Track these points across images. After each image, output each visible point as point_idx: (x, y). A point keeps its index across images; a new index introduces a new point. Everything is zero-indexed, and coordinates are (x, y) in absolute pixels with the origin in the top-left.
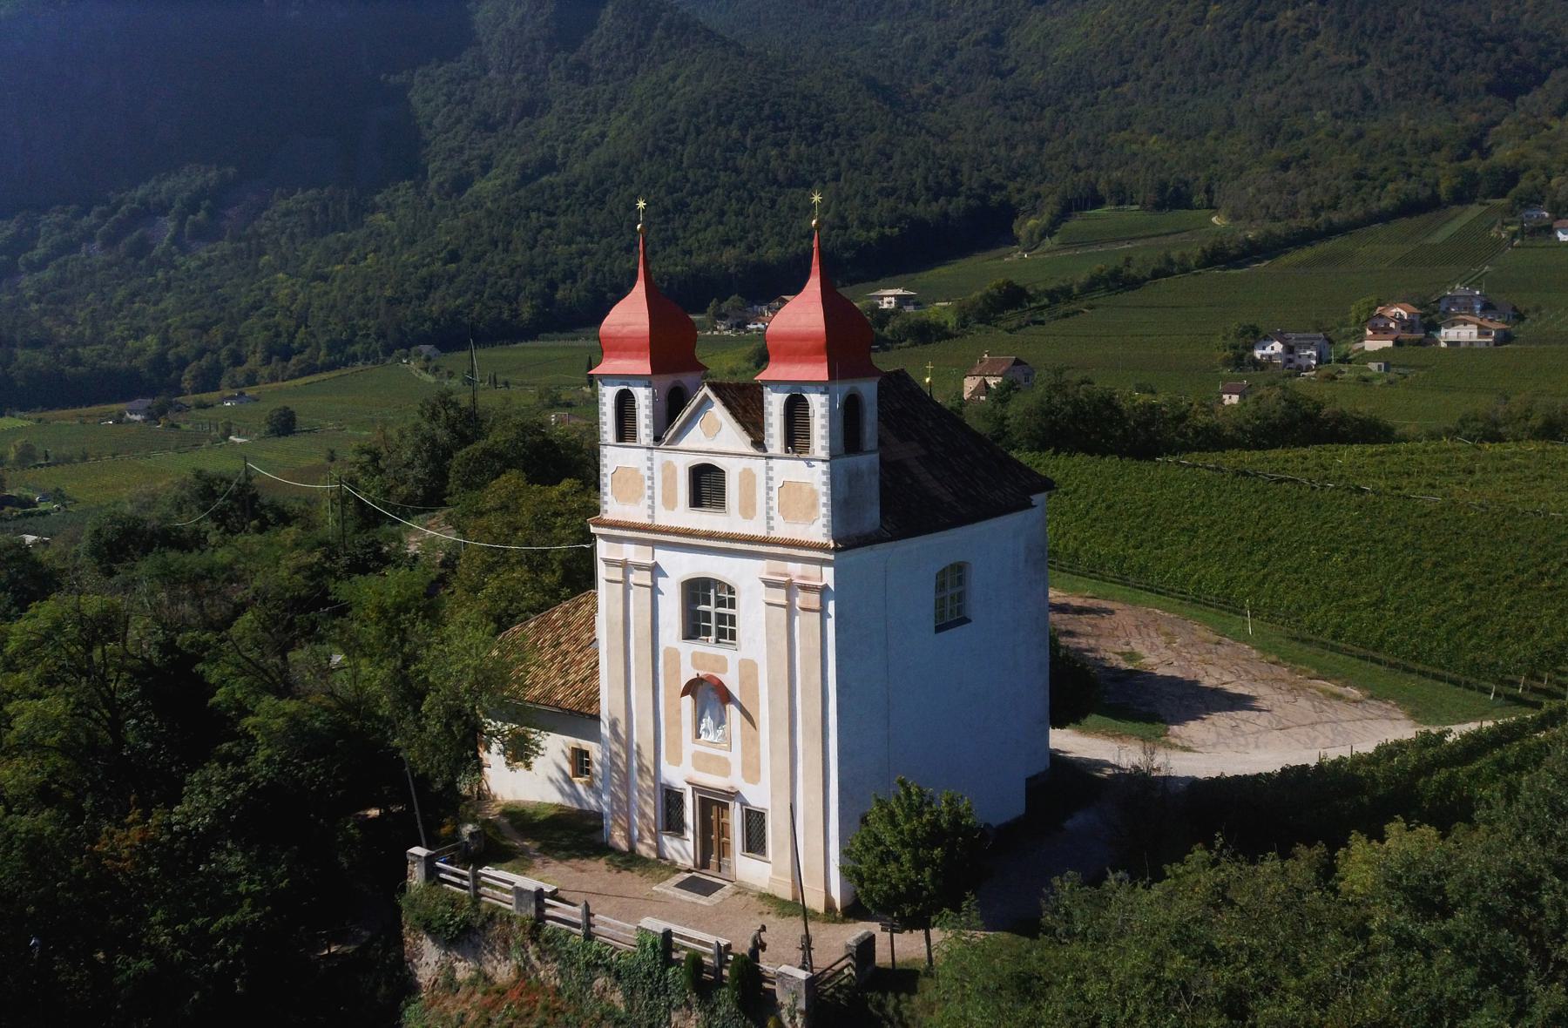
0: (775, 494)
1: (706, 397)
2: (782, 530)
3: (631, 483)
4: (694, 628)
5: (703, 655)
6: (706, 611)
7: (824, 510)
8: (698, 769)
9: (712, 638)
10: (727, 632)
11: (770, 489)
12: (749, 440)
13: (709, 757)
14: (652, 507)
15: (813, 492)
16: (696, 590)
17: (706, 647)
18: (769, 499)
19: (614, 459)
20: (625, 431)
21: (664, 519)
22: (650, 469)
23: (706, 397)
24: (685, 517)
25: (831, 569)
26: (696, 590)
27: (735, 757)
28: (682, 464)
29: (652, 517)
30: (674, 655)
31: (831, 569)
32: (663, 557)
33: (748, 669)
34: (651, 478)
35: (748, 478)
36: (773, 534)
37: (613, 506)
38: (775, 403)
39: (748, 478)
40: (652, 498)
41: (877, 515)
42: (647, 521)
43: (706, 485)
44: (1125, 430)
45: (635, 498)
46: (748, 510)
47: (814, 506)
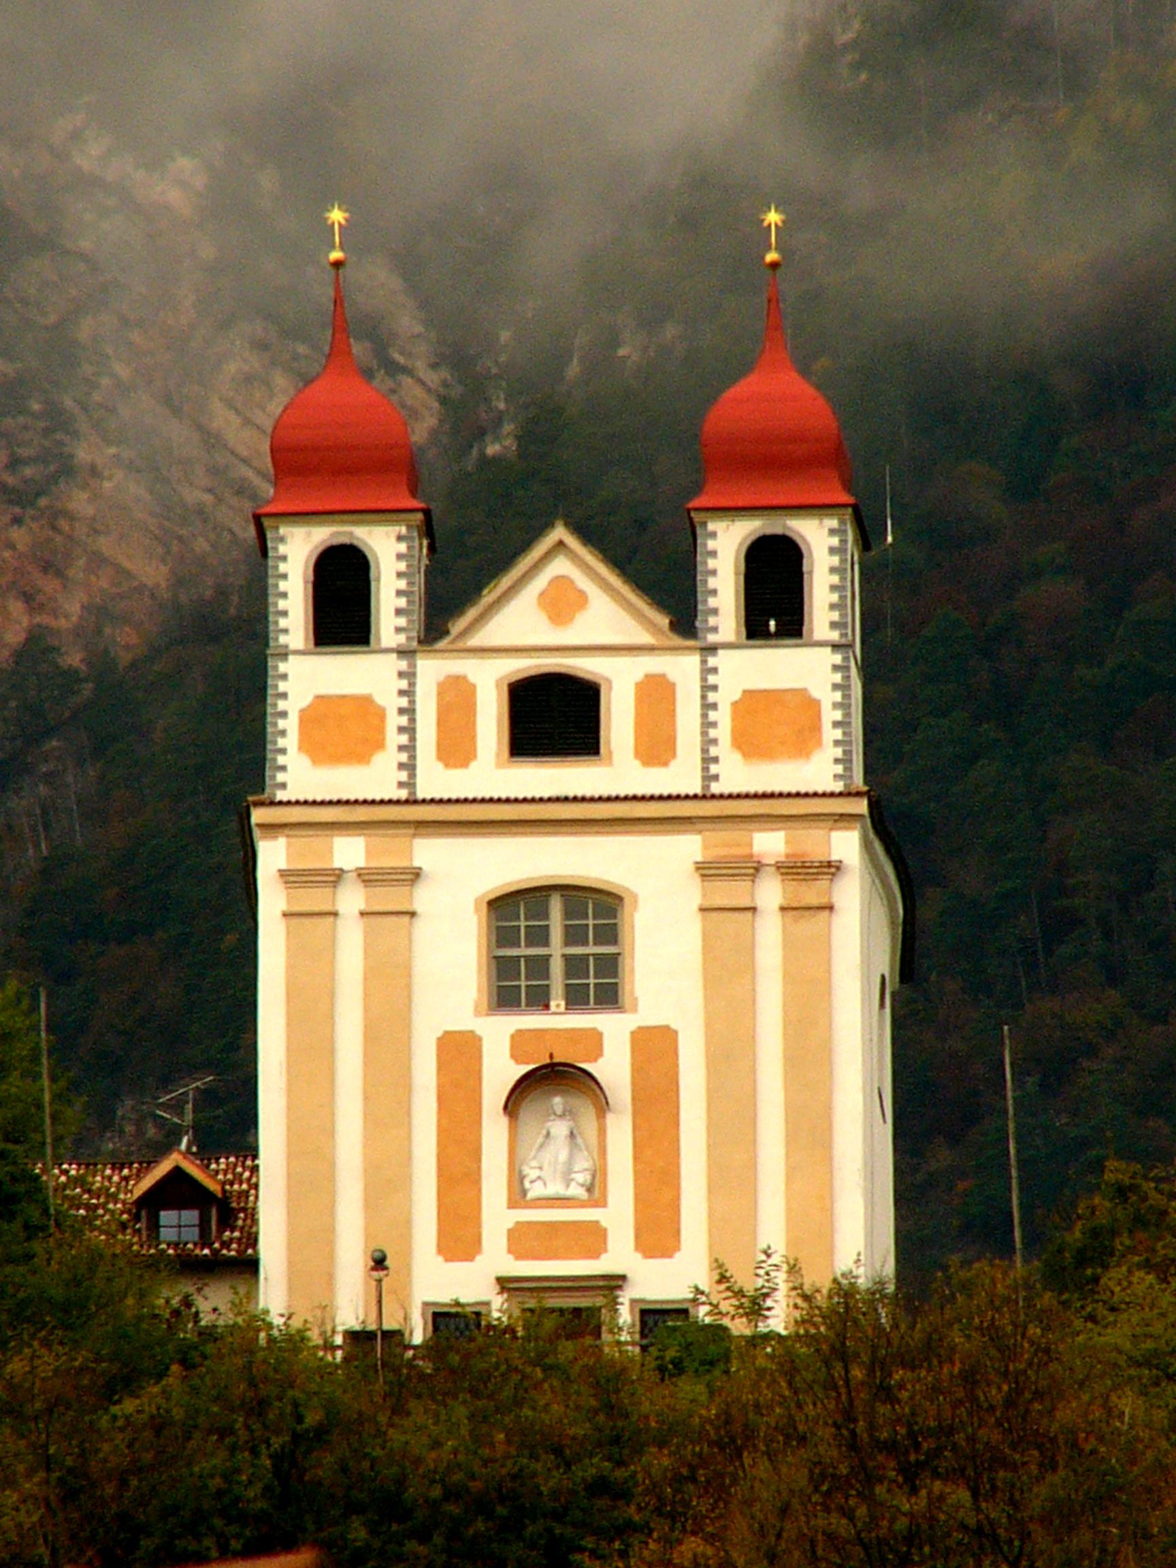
0: (394, 738)
1: (561, 543)
2: (736, 774)
3: (346, 729)
4: (512, 985)
5: (540, 1033)
6: (555, 944)
7: (832, 734)
8: (519, 1257)
9: (558, 1003)
10: (600, 985)
11: (708, 706)
12: (663, 621)
13: (553, 1228)
14: (409, 767)
15: (813, 706)
16: (514, 912)
17: (559, 1020)
18: (707, 725)
19: (306, 677)
20: (342, 609)
21: (436, 780)
22: (408, 693)
23: (561, 543)
24: (493, 773)
25: (162, 1213)
26: (514, 912)
27: (618, 1215)
28: (489, 683)
29: (410, 784)
30: (459, 1052)
31: (162, 1213)
32: (428, 852)
33: (655, 1048)
34: (409, 711)
35: (656, 696)
36: (715, 788)
37: (297, 773)
38: (725, 546)
39: (656, 696)
40: (409, 748)
41: (752, 378)
42: (403, 794)
43: (554, 715)
44: (68, 1178)
45: (754, 704)
46: (656, 746)
47: (816, 727)
